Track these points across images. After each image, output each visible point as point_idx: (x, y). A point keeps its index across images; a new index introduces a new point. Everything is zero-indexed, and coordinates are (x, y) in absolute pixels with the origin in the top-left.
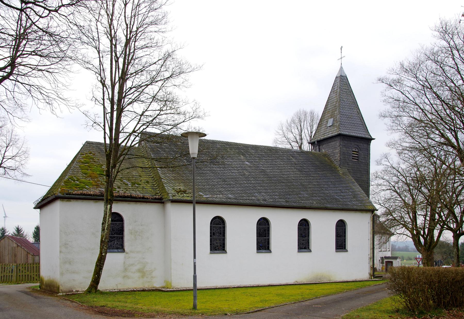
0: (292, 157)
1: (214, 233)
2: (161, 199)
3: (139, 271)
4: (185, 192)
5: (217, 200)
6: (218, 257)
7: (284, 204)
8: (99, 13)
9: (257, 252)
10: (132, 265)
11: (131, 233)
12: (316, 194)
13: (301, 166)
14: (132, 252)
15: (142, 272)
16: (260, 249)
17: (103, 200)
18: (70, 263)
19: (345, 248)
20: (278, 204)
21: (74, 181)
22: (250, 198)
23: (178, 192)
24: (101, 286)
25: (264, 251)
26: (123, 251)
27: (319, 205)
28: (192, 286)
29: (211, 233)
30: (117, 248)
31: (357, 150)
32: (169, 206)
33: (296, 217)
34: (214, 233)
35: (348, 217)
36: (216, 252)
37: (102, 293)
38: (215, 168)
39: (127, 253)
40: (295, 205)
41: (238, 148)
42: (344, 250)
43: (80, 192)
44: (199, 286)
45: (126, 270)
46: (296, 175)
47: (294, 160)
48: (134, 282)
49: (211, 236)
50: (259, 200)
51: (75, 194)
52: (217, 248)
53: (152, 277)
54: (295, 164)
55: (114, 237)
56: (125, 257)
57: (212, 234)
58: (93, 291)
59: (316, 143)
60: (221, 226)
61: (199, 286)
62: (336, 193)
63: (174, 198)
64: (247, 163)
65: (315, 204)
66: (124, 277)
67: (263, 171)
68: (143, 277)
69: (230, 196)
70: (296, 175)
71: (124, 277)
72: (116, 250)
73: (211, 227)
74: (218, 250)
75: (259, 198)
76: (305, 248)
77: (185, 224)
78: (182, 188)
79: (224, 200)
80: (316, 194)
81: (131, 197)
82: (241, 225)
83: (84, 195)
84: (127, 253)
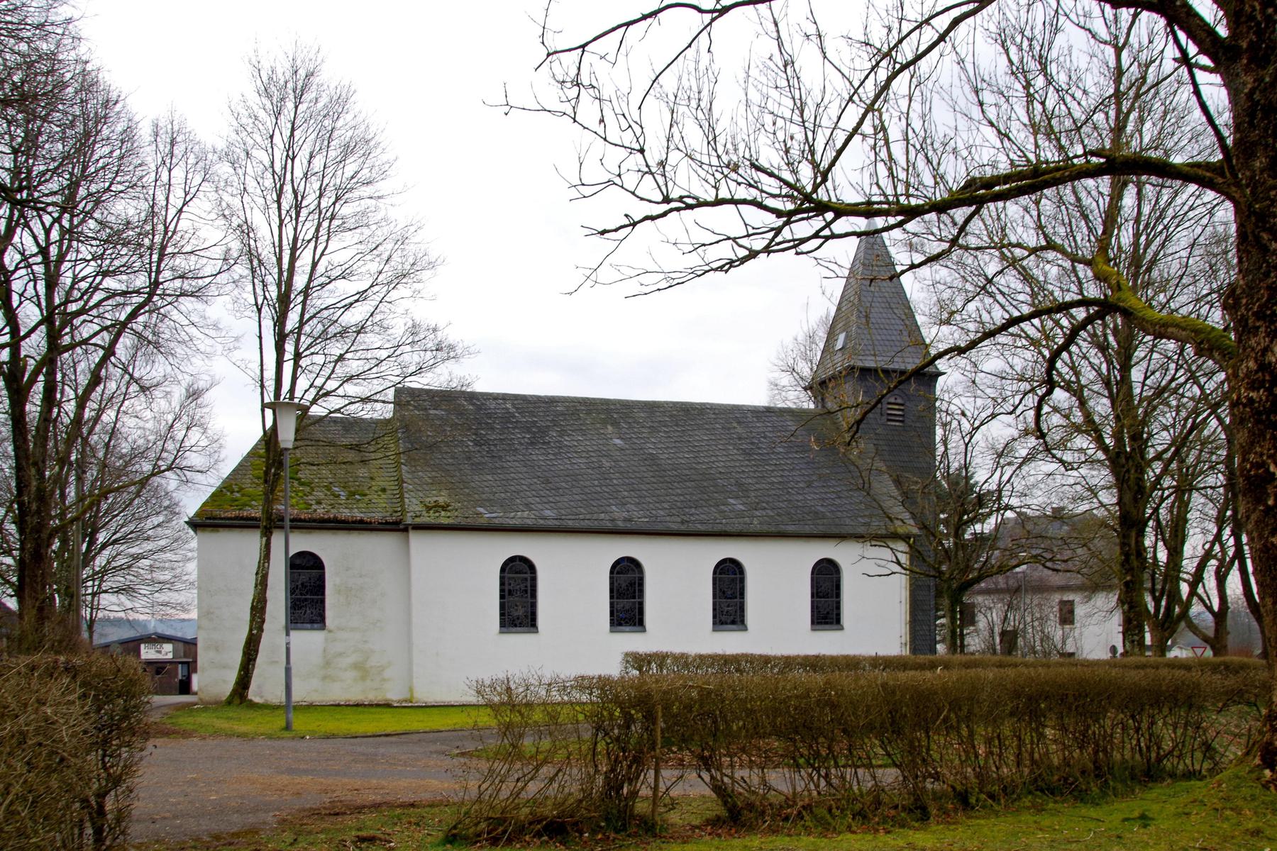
0: (739, 423)
1: (510, 591)
2: (397, 523)
3: (356, 666)
4: (445, 508)
5: (514, 522)
6: (519, 641)
7: (674, 527)
8: (652, 174)
9: (714, 630)
10: (341, 654)
11: (339, 592)
12: (767, 503)
13: (752, 443)
14: (340, 629)
15: (362, 670)
16: (620, 624)
17: (258, 527)
18: (217, 649)
19: (838, 621)
20: (660, 527)
21: (232, 492)
22: (595, 516)
23: (429, 509)
24: (253, 694)
25: (628, 628)
26: (323, 627)
27: (765, 528)
28: (284, 699)
29: (502, 591)
30: (312, 622)
31: (899, 401)
32: (416, 539)
33: (702, 558)
34: (510, 591)
35: (844, 554)
36: (514, 629)
37: (253, 705)
38: (537, 455)
39: (330, 631)
40: (577, 525)
41: (608, 411)
42: (835, 626)
43: (233, 514)
44: (297, 696)
45: (328, 664)
46: (732, 464)
47: (739, 430)
48: (346, 689)
49: (502, 597)
50: (613, 520)
51: (231, 519)
52: (517, 622)
53: (384, 680)
54: (740, 439)
55: (306, 600)
56: (326, 640)
57: (505, 593)
58: (237, 701)
59: (818, 387)
60: (528, 576)
61: (297, 696)
62: (823, 499)
63: (418, 520)
64: (618, 441)
65: (756, 525)
66: (324, 678)
67: (653, 458)
68: (363, 678)
69: (548, 513)
70: (732, 464)
71: (324, 678)
72: (309, 626)
73: (714, 579)
74: (521, 625)
75: (616, 515)
76: (733, 622)
77: (462, 572)
78: (441, 500)
79: (529, 522)
80: (767, 503)
81: (335, 520)
82: (573, 576)
83: (242, 518)
84: (330, 631)
